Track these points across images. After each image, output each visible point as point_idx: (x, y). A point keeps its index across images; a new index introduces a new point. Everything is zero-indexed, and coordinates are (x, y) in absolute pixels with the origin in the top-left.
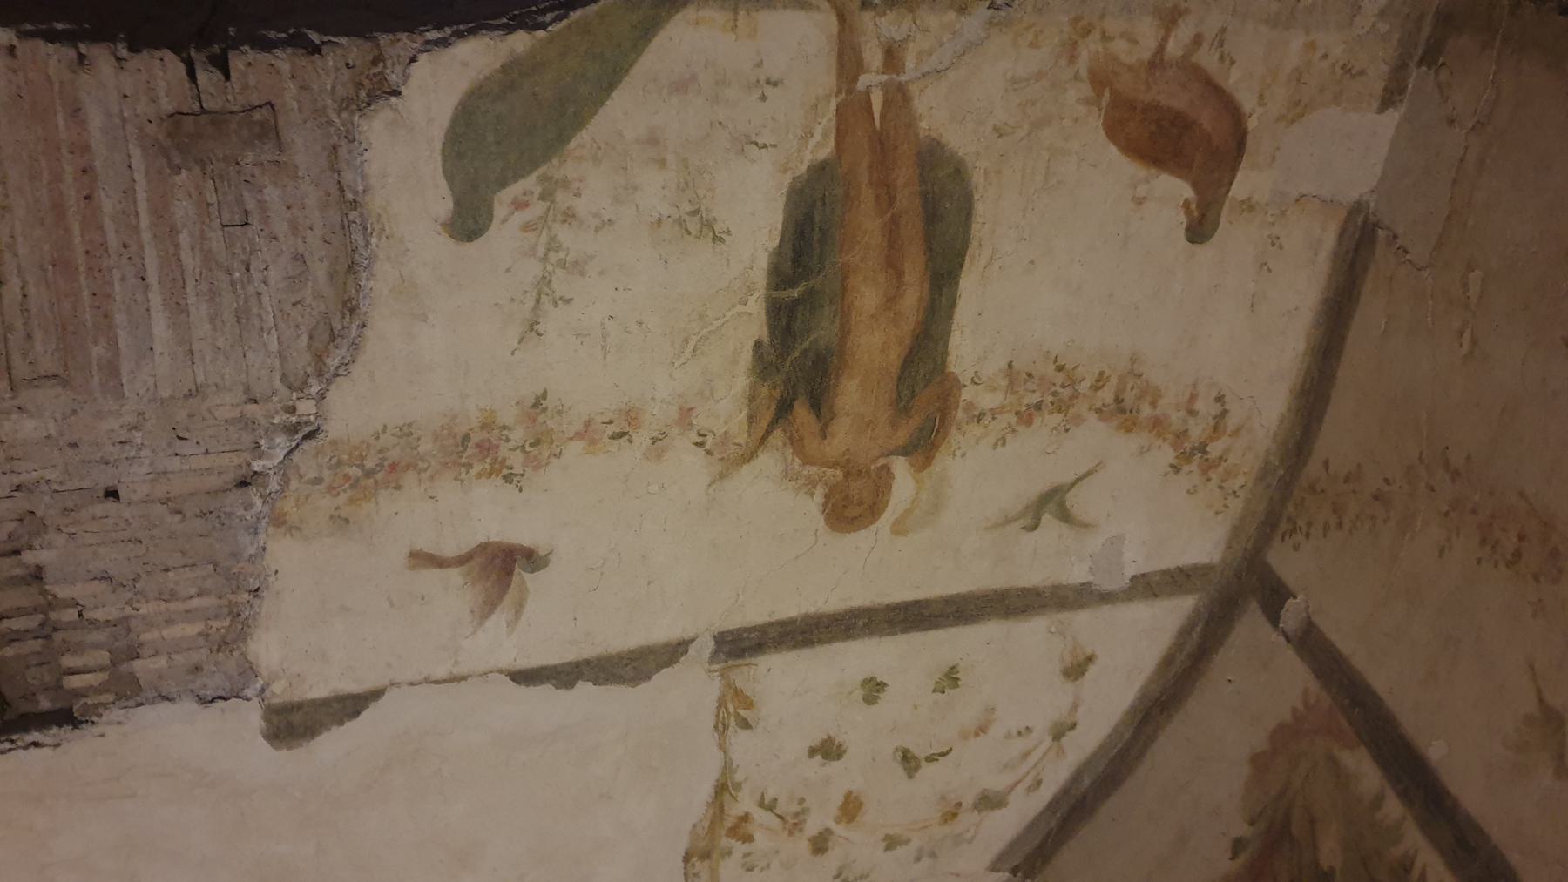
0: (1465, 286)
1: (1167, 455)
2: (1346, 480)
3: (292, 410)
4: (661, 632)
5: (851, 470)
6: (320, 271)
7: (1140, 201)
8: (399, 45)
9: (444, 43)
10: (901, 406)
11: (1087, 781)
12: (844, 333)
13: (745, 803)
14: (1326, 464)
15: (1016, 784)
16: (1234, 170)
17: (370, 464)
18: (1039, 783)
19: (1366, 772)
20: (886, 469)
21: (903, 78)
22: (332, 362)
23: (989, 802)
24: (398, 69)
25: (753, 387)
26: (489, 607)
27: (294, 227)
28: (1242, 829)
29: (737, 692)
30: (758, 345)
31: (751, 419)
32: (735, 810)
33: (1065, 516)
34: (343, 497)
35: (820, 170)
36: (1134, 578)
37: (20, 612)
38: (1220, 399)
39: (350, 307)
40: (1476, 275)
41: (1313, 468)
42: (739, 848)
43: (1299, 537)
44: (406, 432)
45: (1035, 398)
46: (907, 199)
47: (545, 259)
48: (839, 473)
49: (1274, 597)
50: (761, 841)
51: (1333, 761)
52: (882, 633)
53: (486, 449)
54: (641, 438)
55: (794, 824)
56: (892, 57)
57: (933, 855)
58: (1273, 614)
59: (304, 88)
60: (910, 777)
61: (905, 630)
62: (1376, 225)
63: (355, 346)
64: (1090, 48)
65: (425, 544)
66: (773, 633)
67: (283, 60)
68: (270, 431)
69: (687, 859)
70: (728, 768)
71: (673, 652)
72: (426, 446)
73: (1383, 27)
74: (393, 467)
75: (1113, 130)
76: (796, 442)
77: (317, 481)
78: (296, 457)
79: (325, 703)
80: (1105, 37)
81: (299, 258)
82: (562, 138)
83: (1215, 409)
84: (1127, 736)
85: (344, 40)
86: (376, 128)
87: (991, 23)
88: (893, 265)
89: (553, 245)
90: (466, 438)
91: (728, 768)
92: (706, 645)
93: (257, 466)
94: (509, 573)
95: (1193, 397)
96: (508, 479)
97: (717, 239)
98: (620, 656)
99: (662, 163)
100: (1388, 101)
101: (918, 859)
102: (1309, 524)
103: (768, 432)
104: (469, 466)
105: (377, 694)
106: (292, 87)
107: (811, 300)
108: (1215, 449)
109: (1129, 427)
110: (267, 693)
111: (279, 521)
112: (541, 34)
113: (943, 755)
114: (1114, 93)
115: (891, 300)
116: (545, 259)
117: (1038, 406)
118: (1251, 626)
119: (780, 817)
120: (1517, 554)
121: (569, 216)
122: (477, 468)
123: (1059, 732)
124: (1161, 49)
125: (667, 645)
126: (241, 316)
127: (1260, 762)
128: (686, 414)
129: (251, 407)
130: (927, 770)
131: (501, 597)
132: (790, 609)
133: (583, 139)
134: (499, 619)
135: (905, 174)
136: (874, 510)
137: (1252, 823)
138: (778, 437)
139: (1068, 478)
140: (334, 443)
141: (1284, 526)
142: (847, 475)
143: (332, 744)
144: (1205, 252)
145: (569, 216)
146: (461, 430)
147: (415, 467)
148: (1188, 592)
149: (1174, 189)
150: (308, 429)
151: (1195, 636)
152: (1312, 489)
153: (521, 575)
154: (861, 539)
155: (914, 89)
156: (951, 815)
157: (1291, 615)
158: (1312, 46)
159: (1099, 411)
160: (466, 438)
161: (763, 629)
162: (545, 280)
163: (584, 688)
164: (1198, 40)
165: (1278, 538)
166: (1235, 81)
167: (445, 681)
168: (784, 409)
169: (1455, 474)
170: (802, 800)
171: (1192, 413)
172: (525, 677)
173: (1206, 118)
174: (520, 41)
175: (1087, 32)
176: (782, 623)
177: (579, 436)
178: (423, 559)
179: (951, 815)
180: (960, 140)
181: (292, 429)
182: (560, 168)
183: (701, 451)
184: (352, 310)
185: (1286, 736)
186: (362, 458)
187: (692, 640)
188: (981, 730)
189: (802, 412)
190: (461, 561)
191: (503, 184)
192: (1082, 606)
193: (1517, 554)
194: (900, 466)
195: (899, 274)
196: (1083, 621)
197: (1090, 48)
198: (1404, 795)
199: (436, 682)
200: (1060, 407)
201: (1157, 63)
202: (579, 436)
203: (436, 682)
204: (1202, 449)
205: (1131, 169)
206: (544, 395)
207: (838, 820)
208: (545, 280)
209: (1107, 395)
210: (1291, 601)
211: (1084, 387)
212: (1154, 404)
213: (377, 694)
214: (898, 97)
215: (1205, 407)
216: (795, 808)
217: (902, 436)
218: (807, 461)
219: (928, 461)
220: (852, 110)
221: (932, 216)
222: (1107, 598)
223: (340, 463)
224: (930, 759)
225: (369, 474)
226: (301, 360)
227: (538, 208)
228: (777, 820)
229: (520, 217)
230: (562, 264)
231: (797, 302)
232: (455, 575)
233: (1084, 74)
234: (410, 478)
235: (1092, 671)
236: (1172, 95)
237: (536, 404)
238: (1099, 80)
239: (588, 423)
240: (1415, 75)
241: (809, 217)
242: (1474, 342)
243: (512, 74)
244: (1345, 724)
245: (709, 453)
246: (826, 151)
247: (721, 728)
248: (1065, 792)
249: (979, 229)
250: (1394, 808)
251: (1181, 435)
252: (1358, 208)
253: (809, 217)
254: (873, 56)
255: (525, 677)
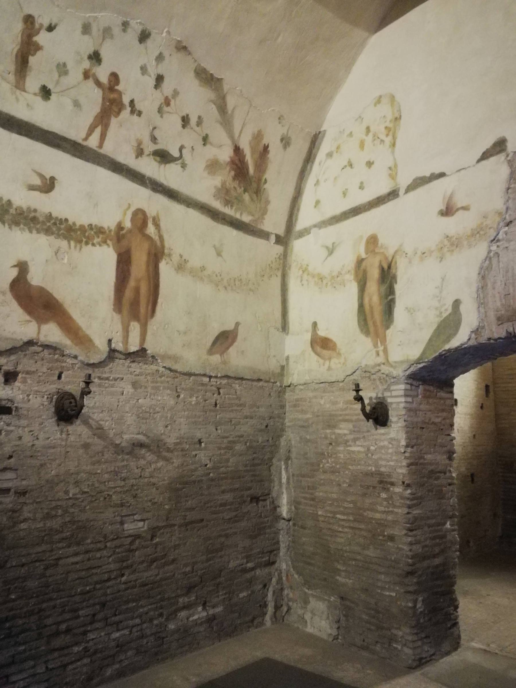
0: (261, 326)
1: (310, 269)
2: (271, 275)
3: (498, 246)
4: (411, 194)
5: (373, 251)
6: (490, 285)
7: (327, 329)
8: (472, 343)
9: (462, 345)
10: (365, 272)
11: (309, 167)
12: (379, 290)
13: (388, 140)
14: (277, 276)
15: (324, 163)
16: (311, 339)
17: (478, 235)
18: (320, 164)
19: (246, 218)
20: (367, 254)
21: (375, 350)
22: (487, 262)
23: (330, 155)
24: (472, 337)
25: (396, 272)
26: (451, 197)
27: (494, 297)
28: (266, 186)
29: (393, 179)
30: (396, 283)
31: (396, 263)
32: (390, 138)
33: (327, 248)
34: (485, 224)
35: (388, 327)
36: (310, 233)
37: (60, 549)
38: (303, 285)
39: (483, 277)
40: (260, 329)
41: (279, 274)
42: (388, 124)
43: (277, 256)
44: (470, 246)
45: (339, 278)
46: (370, 323)
47: (441, 298)
48: (376, 251)
49: (279, 240)
50: (382, 128)
51: (253, 215)
52: (361, 205)
53: (452, 244)
54: (419, 253)
55: (376, 137)
56: (378, 354)
57: (340, 132)
58: (278, 237)
59: (491, 330)
60: (349, 159)
61: (356, 207)
62: (283, 332)
63: (481, 268)
64: (342, 360)
65: (466, 212)
66: (386, 200)
67: (496, 336)
68: (503, 239)
69: (400, 116)
70: (393, 152)
71: (410, 189)
72: (465, 243)
73: (293, 372)
74: (472, 236)
75: (335, 345)
76: (386, 258)
77: (490, 228)
78: (495, 234)
79: (492, 155)
80: (340, 363)
81: (494, 288)
82: (438, 327)
83: (303, 282)
84: (302, 185)
85: (484, 342)
86: (475, 324)
87: (361, 363)
88: (371, 307)
89: (439, 301)
90: (457, 247)
91: (393, 152)
92: (402, 192)
93: (507, 228)
94: (447, 208)
95: (308, 284)
96: (448, 237)
97: (407, 308)
98: (420, 186)
99: (419, 324)
100: (288, 358)
101: (344, 130)
102: (276, 261)
103: (392, 260)
104: (456, 239)
105: (479, 161)
106: (494, 330)
107: (387, 296)
108: (301, 272)
109: (319, 274)
110: (506, 155)
111: (500, 214)
112: (443, 349)
113: (343, 168)
114: (336, 352)
115: (370, 300)
116: (441, 298)
117: (338, 277)
118: (281, 231)
119: (378, 138)
120: (235, 281)
121: (437, 309)
122: (454, 238)
123: (317, 183)
124: (330, 362)
125: (410, 191)
126: (507, 272)
127: (268, 202)
128: (410, 262)
129: (507, 245)
130: (345, 163)
131: (449, 200)
132: (383, 208)
133: (435, 327)
134: (449, 193)
135: (372, 329)
136: (368, 242)
137: (264, 189)
138: (390, 259)
139: (328, 258)
140: (485, 240)
141: (282, 257)
142: (374, 251)
143: (488, 143)
144: (313, 320)
145: (437, 309)
146: (458, 249)
147: (468, 237)
148: (298, 231)
149: (322, 333)
150: (495, 241)
151: (294, 221)
152: (278, 269)
153: (443, 208)
154: (370, 233)
155: (373, 347)
156: (338, 148)
157: (273, 238)
158: (304, 366)
159: (325, 278)
160: (457, 247)
161: (389, 200)
162: (441, 292)
163: (428, 174)
164: (324, 365)
165: (282, 254)
166: (315, 357)
167: (461, 170)
168: (389, 267)
169: (250, 290)
170: (374, 145)
171: (307, 280)
172: (442, 175)
173: (318, 349)
174: (447, 347)
175: (344, 364)
176: (385, 203)
177: (432, 252)
178: (465, 208)
179: (338, 148)
180: (362, 337)
181: (498, 241)
182: (438, 320)
183: (406, 252)
184: (483, 277)
185: (264, 212)
186: (480, 237)
187: (404, 194)
188: (335, 178)
189: (386, 267)
190: (458, 210)
191: (450, 314)
192: (319, 222)
193: (235, 281)
194: (364, 256)
195: (370, 305)
196: (318, 219)
197: (342, 360)
198: (237, 219)
199: (464, 169)
200: (333, 277)
201: (330, 359)
202: (432, 252)
203: (464, 169)
204: (303, 272)
205: (330, 336)
206: (440, 261)
207: (364, 140)
208: (441, 292)
209: (325, 282)
210: (274, 241)
211: (329, 284)
212: (315, 281)
213: (479, 161)
214: (375, 346)
215: (305, 282)
216: (375, 142)
217: (364, 264)
218: (383, 253)
219: (358, 257)
220: (384, 341)
221: (365, 320)
222: (315, 226)
223: (485, 234)
224: (346, 166)
225: (478, 233)
226: (494, 261)
227: (443, 310)
228: (380, 137)
229: (446, 307)
230: (437, 297)
231: (389, 295)
232: (459, 205)
233: (342, 355)
234: (469, 233)
235: (314, 204)
236: (325, 352)
237: (442, 258)
238: (339, 354)
239: (431, 256)
240: (284, 363)
241: (389, 317)
242: (256, 316)
243: (448, 339)
244: (253, 225)
245: (404, 252)
246: (388, 332)
247: (396, 165)
248: (313, 163)
249: (356, 318)
250: (238, 216)
251: (308, 274)
252: (287, 334)
253: (389, 317)
254: (381, 353)
255: (442, 175)
